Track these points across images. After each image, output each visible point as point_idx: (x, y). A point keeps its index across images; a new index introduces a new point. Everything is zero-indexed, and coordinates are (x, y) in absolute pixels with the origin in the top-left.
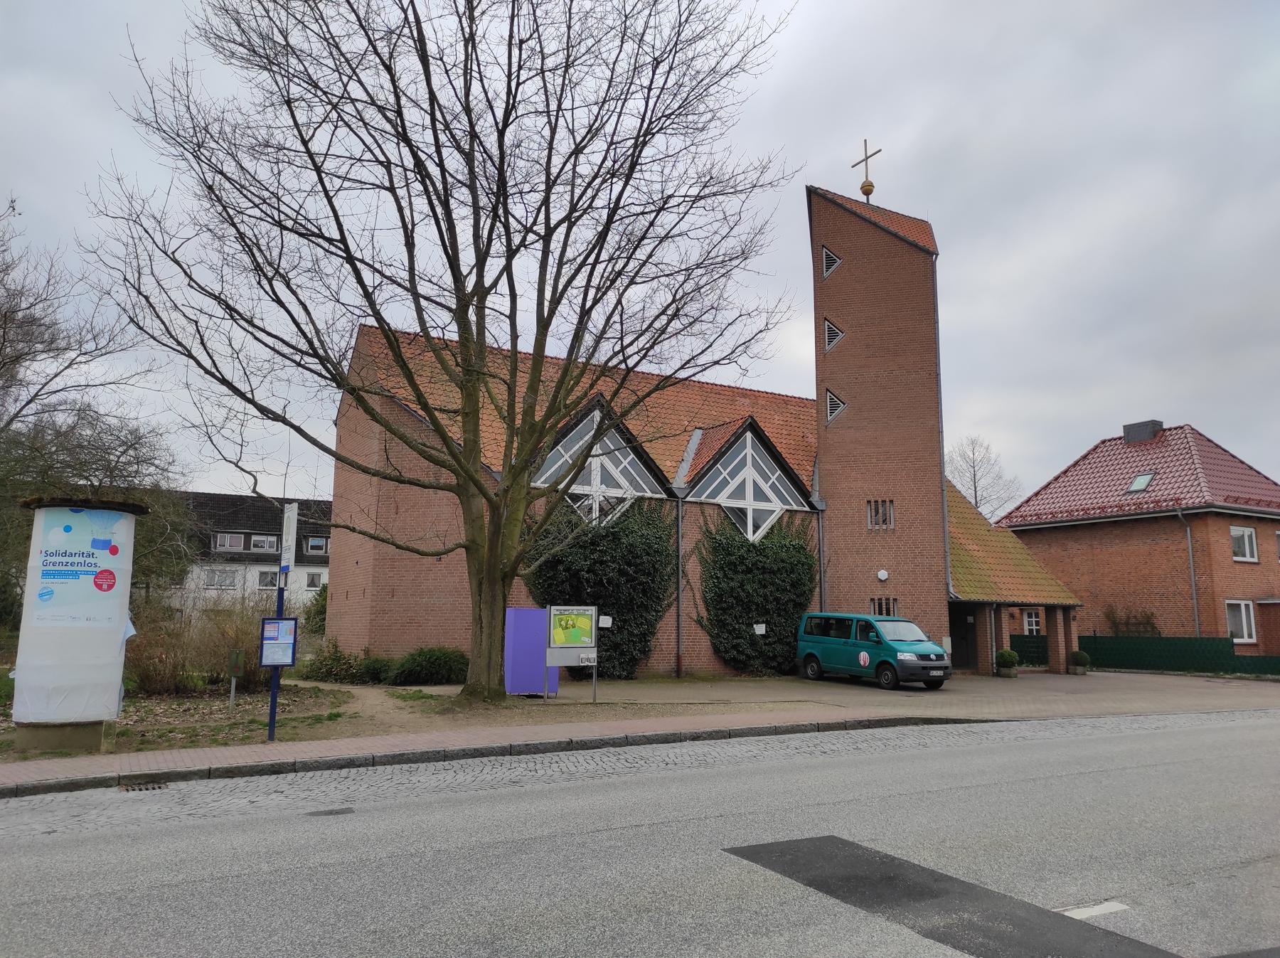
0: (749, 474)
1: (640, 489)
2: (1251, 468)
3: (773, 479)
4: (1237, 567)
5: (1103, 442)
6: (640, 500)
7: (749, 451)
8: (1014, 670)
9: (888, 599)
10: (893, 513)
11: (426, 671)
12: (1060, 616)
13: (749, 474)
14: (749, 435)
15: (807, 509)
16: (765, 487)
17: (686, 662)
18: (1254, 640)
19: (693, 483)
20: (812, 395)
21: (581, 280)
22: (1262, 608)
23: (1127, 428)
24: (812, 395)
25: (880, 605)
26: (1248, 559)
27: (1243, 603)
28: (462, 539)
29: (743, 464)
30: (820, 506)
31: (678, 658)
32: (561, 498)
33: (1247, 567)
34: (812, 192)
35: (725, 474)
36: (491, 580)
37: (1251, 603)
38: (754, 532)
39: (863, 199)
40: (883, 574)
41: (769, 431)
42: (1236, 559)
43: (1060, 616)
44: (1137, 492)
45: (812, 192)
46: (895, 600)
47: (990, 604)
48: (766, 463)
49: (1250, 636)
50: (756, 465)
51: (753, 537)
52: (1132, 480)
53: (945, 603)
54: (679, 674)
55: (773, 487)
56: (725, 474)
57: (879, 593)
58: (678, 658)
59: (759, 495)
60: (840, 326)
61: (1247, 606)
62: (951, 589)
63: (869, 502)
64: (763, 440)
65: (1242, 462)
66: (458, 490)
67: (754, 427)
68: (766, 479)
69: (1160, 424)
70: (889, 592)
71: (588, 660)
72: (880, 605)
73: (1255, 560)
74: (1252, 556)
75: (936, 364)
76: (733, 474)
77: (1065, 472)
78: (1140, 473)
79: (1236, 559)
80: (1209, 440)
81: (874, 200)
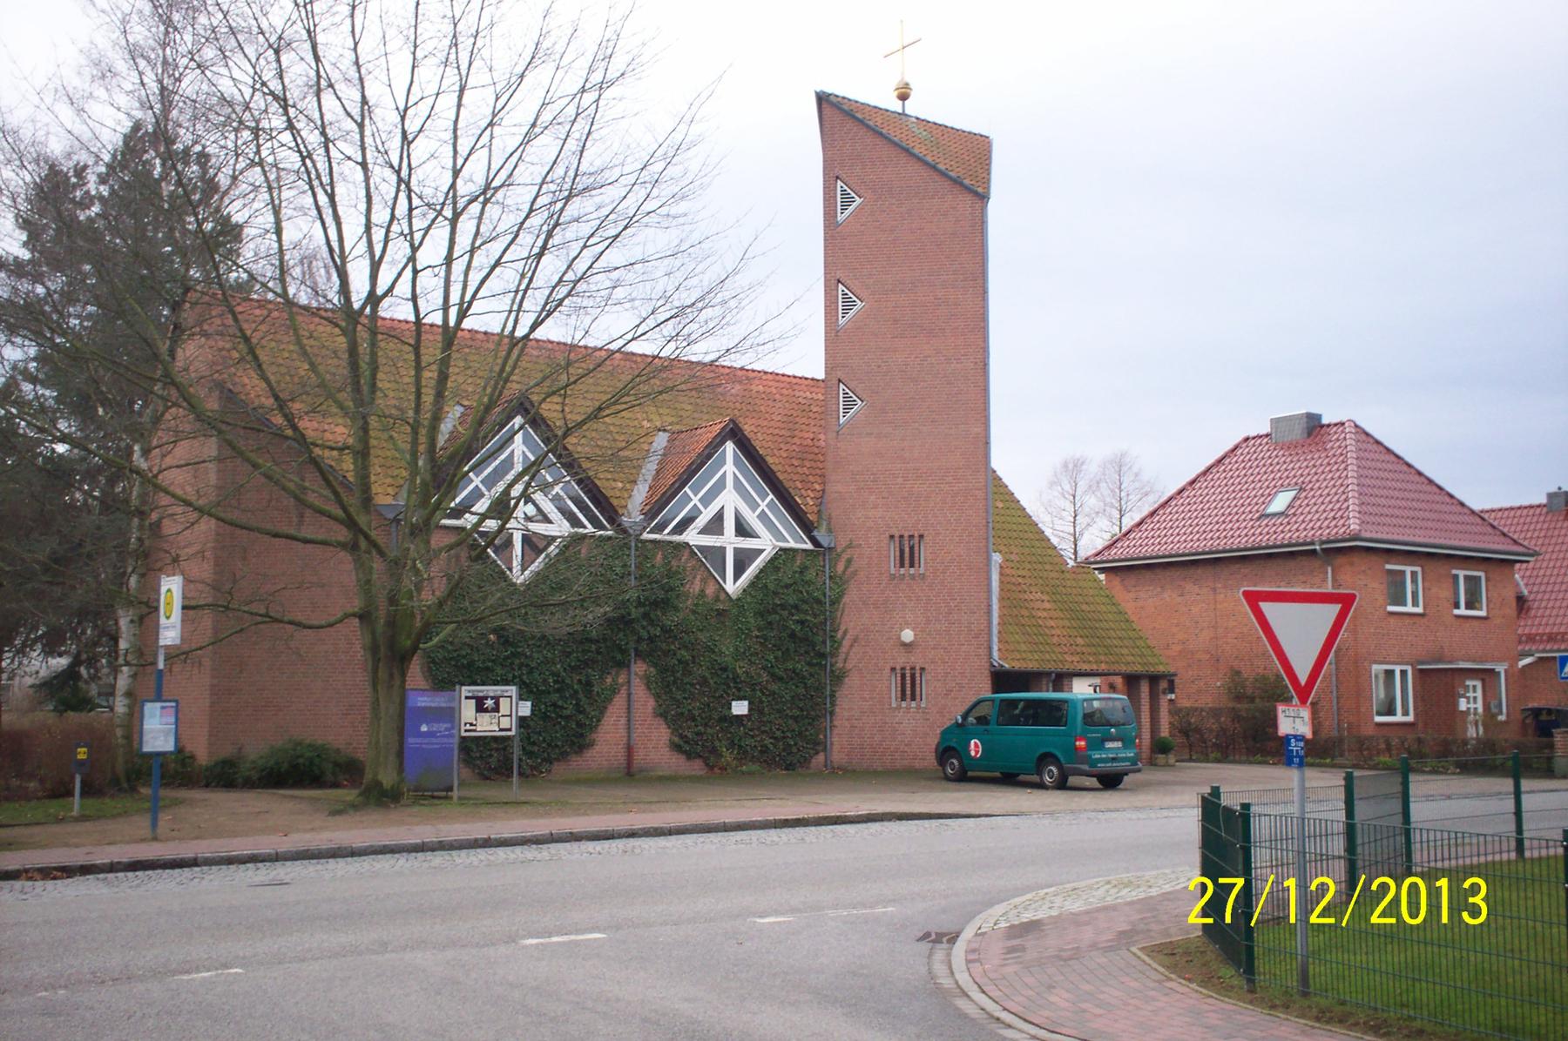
0: (729, 501)
1: (579, 524)
2: (1431, 482)
3: (763, 506)
4: (1392, 620)
5: (1247, 439)
6: (576, 540)
7: (729, 468)
8: (1172, 759)
9: (913, 668)
10: (924, 554)
11: (299, 772)
12: (1145, 688)
13: (729, 501)
14: (730, 447)
15: (809, 546)
16: (752, 518)
17: (639, 757)
18: (1410, 718)
19: (654, 509)
20: (821, 375)
21: (507, 277)
22: (1422, 674)
23: (1275, 422)
24: (821, 375)
25: (903, 677)
26: (1409, 609)
27: (1398, 669)
28: (357, 604)
29: (720, 486)
30: (824, 541)
31: (630, 749)
32: (479, 550)
33: (1408, 621)
34: (823, 99)
35: (695, 500)
36: (392, 651)
37: (1409, 669)
38: (737, 577)
39: (895, 105)
40: (908, 635)
41: (760, 443)
42: (1391, 608)
43: (1145, 688)
44: (1274, 515)
45: (823, 99)
46: (922, 669)
47: (1048, 674)
48: (753, 484)
49: (1406, 713)
50: (738, 486)
51: (733, 587)
52: (1271, 496)
53: (987, 673)
54: (631, 773)
55: (763, 517)
56: (695, 500)
57: (901, 660)
58: (630, 749)
59: (742, 530)
60: (858, 292)
61: (1403, 673)
62: (996, 654)
63: (892, 537)
64: (746, 448)
65: (1420, 474)
66: (353, 547)
67: (734, 433)
68: (753, 505)
69: (1319, 417)
70: (916, 660)
71: (1429, 798)
72: (903, 677)
73: (1419, 610)
74: (1415, 604)
75: (985, 351)
76: (706, 501)
77: (1193, 482)
78: (1283, 488)
79: (1391, 608)
80: (1378, 442)
81: (913, 108)
